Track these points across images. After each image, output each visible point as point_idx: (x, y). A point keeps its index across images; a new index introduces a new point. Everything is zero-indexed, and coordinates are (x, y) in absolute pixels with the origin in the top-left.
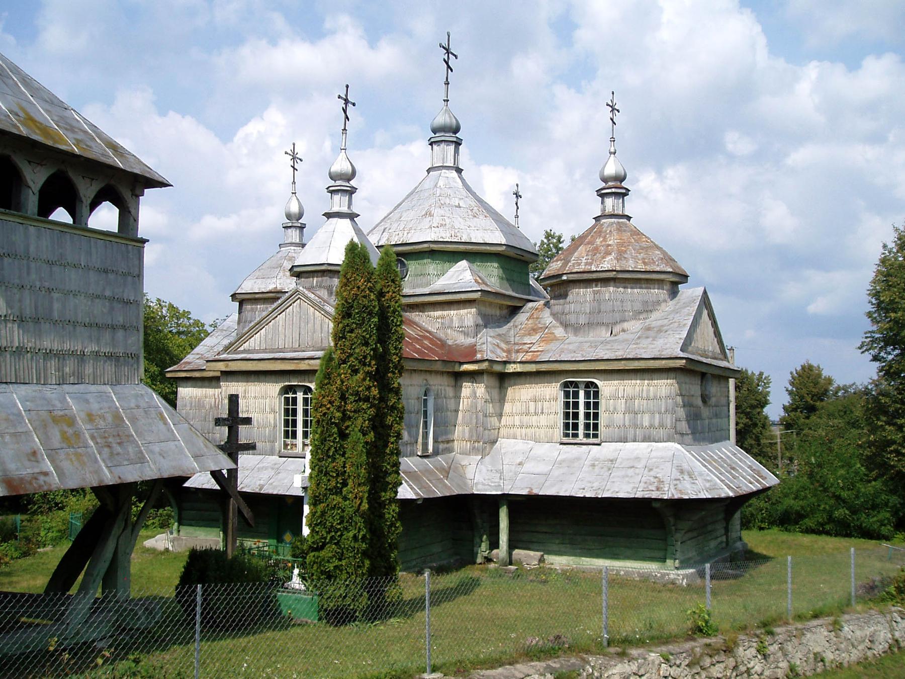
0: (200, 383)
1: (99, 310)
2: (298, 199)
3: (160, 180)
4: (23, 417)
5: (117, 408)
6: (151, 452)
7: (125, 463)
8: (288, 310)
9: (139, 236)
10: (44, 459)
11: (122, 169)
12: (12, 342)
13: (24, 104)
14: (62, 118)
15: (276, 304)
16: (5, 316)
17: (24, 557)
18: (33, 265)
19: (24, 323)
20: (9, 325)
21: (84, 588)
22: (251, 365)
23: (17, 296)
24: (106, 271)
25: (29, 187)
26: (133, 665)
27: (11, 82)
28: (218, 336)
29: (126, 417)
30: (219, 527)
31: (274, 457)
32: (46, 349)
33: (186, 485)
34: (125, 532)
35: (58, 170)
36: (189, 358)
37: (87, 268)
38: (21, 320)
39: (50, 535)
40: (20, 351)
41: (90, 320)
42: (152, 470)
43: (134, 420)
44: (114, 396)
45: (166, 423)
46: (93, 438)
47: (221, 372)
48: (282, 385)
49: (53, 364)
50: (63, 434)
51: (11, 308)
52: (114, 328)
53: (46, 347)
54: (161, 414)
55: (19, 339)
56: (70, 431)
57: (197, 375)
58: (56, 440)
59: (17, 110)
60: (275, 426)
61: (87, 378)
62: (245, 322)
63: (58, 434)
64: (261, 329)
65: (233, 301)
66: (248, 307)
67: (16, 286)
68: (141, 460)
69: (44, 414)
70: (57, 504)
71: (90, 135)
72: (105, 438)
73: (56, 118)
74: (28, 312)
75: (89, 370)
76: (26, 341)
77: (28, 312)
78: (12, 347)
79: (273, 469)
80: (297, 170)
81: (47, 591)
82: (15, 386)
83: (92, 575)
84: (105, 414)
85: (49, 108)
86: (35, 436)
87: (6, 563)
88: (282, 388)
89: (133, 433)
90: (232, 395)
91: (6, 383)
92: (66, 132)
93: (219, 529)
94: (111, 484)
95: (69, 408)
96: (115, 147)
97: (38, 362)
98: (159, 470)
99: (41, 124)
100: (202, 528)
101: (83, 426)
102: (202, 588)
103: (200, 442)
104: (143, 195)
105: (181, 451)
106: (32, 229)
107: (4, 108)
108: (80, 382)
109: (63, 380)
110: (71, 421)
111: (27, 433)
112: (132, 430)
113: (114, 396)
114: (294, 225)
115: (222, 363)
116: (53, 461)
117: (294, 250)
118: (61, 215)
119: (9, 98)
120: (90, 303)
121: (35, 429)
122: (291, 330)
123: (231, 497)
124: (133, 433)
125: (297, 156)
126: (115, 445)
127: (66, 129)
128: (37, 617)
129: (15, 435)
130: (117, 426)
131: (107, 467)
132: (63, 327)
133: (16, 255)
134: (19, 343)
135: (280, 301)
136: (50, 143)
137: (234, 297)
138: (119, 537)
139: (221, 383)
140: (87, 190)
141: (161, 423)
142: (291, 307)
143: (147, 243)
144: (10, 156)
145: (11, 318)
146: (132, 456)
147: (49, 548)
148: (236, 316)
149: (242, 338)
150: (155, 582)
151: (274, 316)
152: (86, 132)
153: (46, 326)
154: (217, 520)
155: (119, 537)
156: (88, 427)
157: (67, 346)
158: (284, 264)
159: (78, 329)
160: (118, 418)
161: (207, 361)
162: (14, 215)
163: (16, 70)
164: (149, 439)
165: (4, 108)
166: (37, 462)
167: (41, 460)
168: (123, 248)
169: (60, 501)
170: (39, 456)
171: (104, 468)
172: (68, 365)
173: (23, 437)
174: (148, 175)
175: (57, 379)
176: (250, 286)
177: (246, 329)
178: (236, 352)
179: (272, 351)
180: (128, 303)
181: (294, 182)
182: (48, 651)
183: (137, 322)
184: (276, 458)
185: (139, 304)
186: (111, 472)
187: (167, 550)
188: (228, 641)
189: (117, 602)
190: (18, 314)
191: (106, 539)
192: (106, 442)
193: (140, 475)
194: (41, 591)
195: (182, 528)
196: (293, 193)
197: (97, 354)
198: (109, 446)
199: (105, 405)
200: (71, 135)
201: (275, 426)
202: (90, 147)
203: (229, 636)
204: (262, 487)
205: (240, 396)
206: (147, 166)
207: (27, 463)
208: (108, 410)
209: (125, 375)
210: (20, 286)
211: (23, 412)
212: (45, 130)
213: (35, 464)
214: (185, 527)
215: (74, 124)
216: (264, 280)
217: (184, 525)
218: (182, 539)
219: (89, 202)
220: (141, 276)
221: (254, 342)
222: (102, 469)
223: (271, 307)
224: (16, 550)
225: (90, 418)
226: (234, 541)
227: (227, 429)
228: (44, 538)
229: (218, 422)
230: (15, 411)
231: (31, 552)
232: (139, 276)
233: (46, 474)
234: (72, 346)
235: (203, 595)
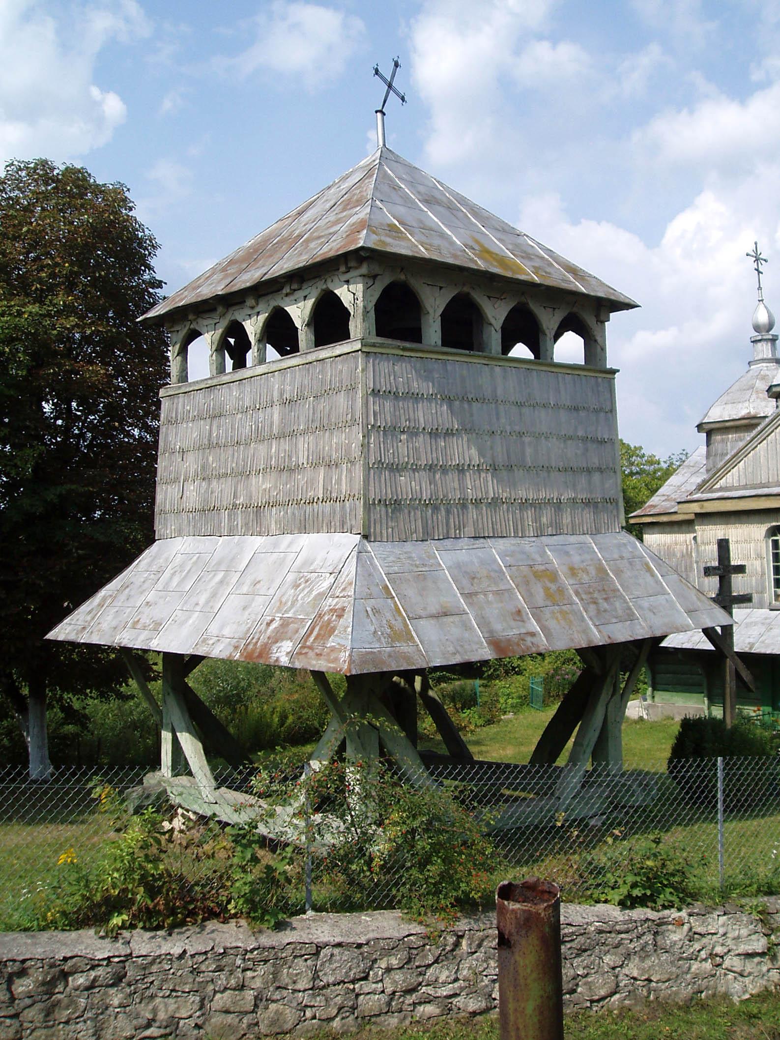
0: (668, 529)
1: (572, 453)
2: (766, 307)
3: (627, 301)
4: (504, 573)
5: (599, 560)
6: (640, 608)
7: (614, 620)
8: (769, 437)
9: (608, 367)
10: (529, 619)
11: (583, 295)
12: (487, 492)
13: (478, 237)
14: (517, 245)
15: (755, 432)
16: (478, 465)
17: (489, 724)
18: (501, 407)
19: (498, 472)
20: (483, 475)
21: (574, 759)
22: (730, 504)
23: (489, 443)
24: (576, 409)
25: (491, 324)
26: (654, 845)
27: (460, 215)
28: (685, 473)
29: (610, 569)
30: (703, 693)
31: (763, 610)
32: (521, 499)
33: (663, 644)
34: (615, 697)
35: (518, 303)
36: (655, 500)
37: (557, 407)
38: (494, 469)
39: (510, 701)
40: (495, 503)
41: (564, 464)
42: (643, 628)
43: (618, 572)
44: (595, 547)
45: (653, 575)
46: (577, 593)
47: (696, 514)
48: (769, 525)
49: (529, 514)
50: (546, 589)
51: (484, 457)
52: (589, 471)
53: (521, 496)
54: (647, 565)
55: (493, 489)
56: (553, 587)
57: (664, 519)
58: (540, 598)
59: (470, 243)
60: (763, 574)
61: (565, 528)
62: (715, 455)
63: (541, 590)
64: (739, 462)
65: (699, 432)
66: (717, 438)
67: (486, 432)
68: (631, 617)
69: (525, 570)
70: (514, 668)
71: (547, 260)
72: (590, 593)
73: (510, 247)
74: (501, 460)
75: (566, 519)
76: (500, 491)
77: (501, 460)
78: (488, 499)
79: (763, 624)
80: (762, 273)
81: (532, 762)
82: (493, 540)
83: (582, 745)
84: (588, 568)
85: (503, 237)
86: (518, 594)
87: (472, 731)
88: (768, 530)
89: (619, 587)
90: (721, 540)
91: (484, 537)
92: (522, 260)
93: (703, 695)
94: (601, 644)
95: (550, 562)
96: (573, 270)
97: (514, 513)
98: (651, 627)
99: (497, 254)
100: (679, 694)
101: (566, 581)
102: (723, 761)
103: (693, 595)
104: (609, 321)
105: (672, 606)
106: (497, 369)
107: (458, 243)
108: (458, 536)
109: (541, 533)
110: (553, 576)
111: (509, 591)
112: (618, 584)
113: (595, 547)
114: (764, 337)
115: (696, 504)
116: (538, 621)
117: (767, 367)
118: (521, 351)
119: (462, 231)
120: (562, 445)
121: (517, 586)
122: (775, 462)
123: (727, 657)
124: (619, 587)
125: (761, 256)
126: (601, 601)
127: (523, 257)
128: (515, 789)
129: (498, 593)
130: (602, 579)
131: (595, 625)
132: (537, 473)
133: (484, 399)
134: (494, 494)
135: (759, 428)
136: (509, 274)
137: (700, 427)
138: (607, 704)
139: (696, 527)
140: (549, 320)
141: (648, 574)
142: (773, 434)
143: (617, 374)
144: (468, 294)
145: (484, 468)
146: (620, 612)
147: (510, 716)
148: (703, 449)
149: (715, 473)
150: (634, 755)
151: (753, 446)
152: (542, 258)
153: (519, 474)
154: (700, 685)
155: (607, 704)
156: (572, 582)
157: (542, 495)
158: (757, 385)
159: (552, 474)
160: (601, 570)
161: (679, 503)
162: (479, 356)
163: (463, 201)
164: (637, 593)
165: (458, 243)
166: (523, 621)
167: (526, 619)
168: (593, 380)
169: (516, 666)
170: (524, 614)
171: (592, 627)
172: (545, 515)
173: (506, 595)
174: (613, 298)
175: (535, 530)
176: (718, 414)
177: (722, 463)
178: (711, 490)
179: (745, 487)
180: (603, 442)
181: (760, 288)
182: (554, 827)
183: (613, 464)
184: (765, 612)
185: (613, 443)
186: (599, 631)
187: (641, 718)
188: (734, 823)
189: (608, 775)
190: (491, 462)
191: (594, 708)
192: (592, 598)
193: (630, 633)
194: (526, 762)
195: (658, 694)
196: (759, 301)
197: (574, 501)
198: (595, 603)
199: (587, 557)
200: (529, 263)
201: (763, 574)
202: (549, 273)
203: (735, 817)
204: (752, 645)
205: (730, 541)
206: (609, 287)
207: (513, 623)
208: (590, 563)
209: (604, 523)
210: (491, 432)
211: (504, 568)
212: (502, 261)
213: (520, 623)
214: (660, 692)
215: (530, 251)
216: (735, 405)
217: (659, 690)
218: (658, 706)
219: (553, 333)
220: (614, 413)
221: (732, 478)
222: (590, 628)
223: (748, 436)
224: (480, 717)
225: (573, 571)
226: (733, 707)
227: (717, 578)
228: (504, 705)
229: (708, 571)
230: (495, 567)
231: (495, 720)
232: (611, 411)
233: (533, 634)
234: (548, 495)
235: (724, 769)
